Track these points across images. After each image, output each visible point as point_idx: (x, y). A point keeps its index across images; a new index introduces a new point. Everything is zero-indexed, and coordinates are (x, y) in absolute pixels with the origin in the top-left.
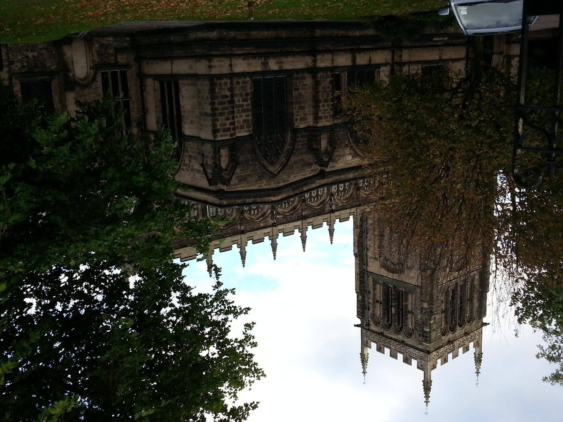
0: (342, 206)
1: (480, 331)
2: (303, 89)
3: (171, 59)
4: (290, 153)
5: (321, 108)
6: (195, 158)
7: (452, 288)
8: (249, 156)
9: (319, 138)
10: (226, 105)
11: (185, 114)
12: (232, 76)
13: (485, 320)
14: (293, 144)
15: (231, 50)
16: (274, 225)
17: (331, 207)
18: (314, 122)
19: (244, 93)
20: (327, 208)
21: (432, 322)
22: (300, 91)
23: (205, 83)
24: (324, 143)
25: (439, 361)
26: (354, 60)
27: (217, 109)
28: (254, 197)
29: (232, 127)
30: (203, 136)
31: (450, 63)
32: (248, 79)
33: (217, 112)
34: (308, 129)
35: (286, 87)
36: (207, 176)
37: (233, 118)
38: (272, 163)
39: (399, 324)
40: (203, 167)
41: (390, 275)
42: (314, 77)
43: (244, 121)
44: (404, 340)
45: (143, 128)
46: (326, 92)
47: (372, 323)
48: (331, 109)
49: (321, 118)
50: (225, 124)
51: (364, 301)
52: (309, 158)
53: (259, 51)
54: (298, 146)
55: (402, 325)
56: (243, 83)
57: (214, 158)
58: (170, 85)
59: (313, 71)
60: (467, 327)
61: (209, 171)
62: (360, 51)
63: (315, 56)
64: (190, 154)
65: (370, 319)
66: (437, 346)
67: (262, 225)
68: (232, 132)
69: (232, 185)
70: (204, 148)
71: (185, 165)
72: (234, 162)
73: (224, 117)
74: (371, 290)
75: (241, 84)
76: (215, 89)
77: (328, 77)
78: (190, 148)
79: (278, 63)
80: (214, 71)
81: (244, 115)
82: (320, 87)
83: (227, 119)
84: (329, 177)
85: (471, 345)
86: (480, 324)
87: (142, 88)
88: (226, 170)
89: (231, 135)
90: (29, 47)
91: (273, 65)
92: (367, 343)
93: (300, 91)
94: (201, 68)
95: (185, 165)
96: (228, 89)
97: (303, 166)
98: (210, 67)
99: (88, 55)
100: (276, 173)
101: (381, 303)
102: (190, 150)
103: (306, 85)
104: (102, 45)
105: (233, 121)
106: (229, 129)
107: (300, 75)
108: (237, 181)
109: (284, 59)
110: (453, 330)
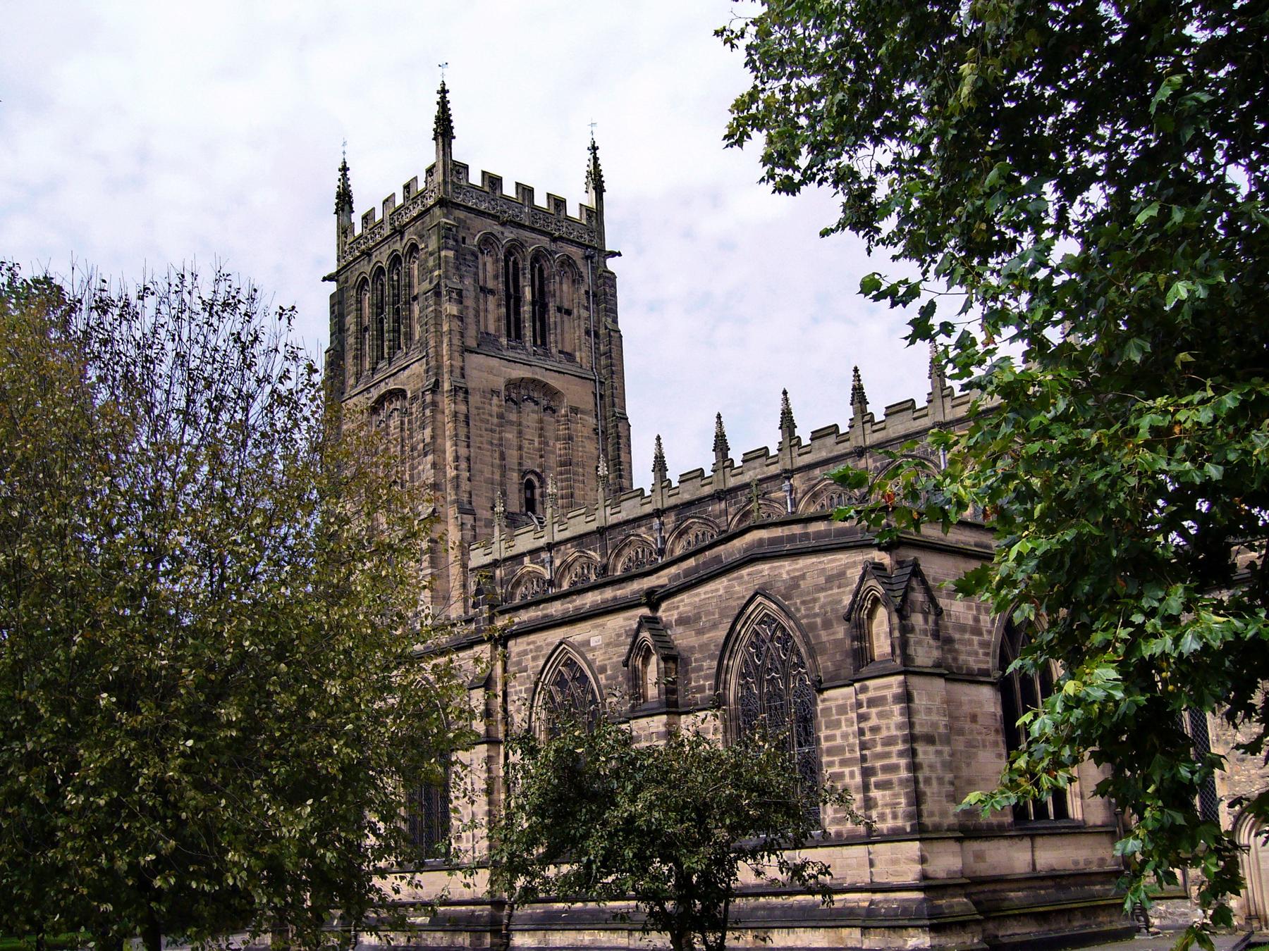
0: (639, 527)
1: (343, 263)
3: (1035, 879)
6: (962, 628)
7: (399, 354)
8: (824, 636)
10: (878, 764)
11: (992, 737)
12: (870, 837)
13: (332, 287)
14: (721, 671)
15: (872, 902)
16: (788, 474)
17: (662, 524)
20: (670, 520)
21: (436, 273)
23: (936, 819)
27: (901, 754)
29: (864, 710)
32: (832, 830)
33: (900, 747)
36: (924, 582)
37: (861, 732)
38: (767, 620)
40: (936, 606)
41: (540, 375)
43: (837, 724)
44: (500, 228)
50: (880, 715)
52: (682, 638)
54: (710, 665)
55: (506, 261)
60: (366, 268)
61: (919, 596)
64: (976, 638)
66: (427, 218)
67: (817, 472)
68: (862, 697)
70: (936, 654)
73: (884, 733)
78: (977, 654)
80: (914, 848)
81: (839, 741)
83: (875, 730)
84: (638, 592)
85: (358, 230)
88: (876, 601)
92: (589, 217)
96: (876, 805)
97: (697, 618)
100: (759, 599)
102: (976, 647)
105: (862, 725)
106: (872, 702)
110: (396, 260)
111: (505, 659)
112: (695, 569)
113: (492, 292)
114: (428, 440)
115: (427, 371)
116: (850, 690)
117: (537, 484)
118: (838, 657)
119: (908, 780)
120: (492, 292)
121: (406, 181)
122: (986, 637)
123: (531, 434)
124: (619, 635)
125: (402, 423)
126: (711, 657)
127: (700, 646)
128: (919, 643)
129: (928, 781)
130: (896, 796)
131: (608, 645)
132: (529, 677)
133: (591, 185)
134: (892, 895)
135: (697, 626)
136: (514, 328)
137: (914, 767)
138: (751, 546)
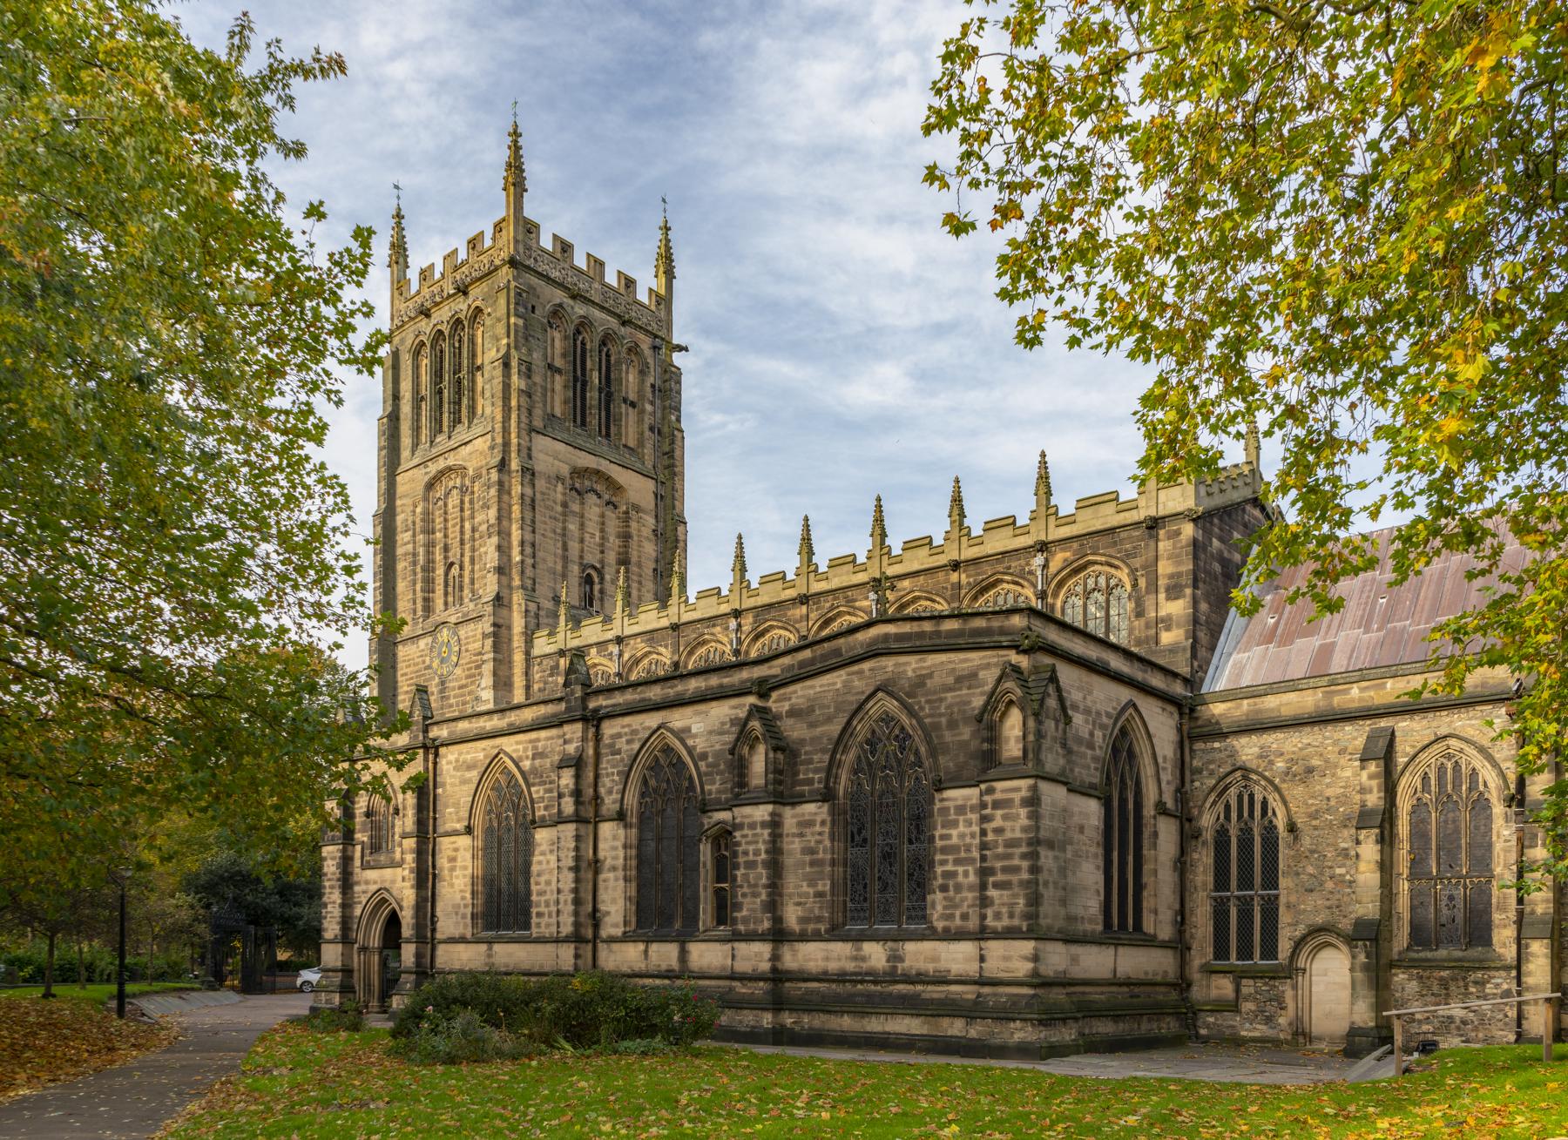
2: (807, 895)
4: (841, 742)
5: (762, 847)
6: (1079, 740)
7: (459, 428)
8: (948, 736)
9: (771, 776)
10: (998, 865)
11: (1093, 849)
12: (982, 934)
14: (833, 765)
15: (979, 995)
17: (739, 625)
18: (780, 815)
19: (951, 893)
20: (748, 622)
22: (811, 891)
23: (1049, 921)
24: (758, 764)
25: (488, 243)
26: (683, 955)
27: (1024, 856)
28: (938, 633)
29: (988, 811)
30: (1061, 791)
31: (469, 935)
33: (1024, 849)
34: (796, 801)
35: (845, 902)
36: (1059, 690)
37: (983, 833)
38: (887, 719)
39: (583, 343)
42: (778, 920)
43: (955, 824)
44: (571, 302)
45: (1187, 825)
46: (750, 886)
47: (647, 352)
48: (738, 844)
49: (764, 825)
50: (1005, 818)
51: (664, 408)
52: (794, 730)
53: (911, 987)
56: (951, 917)
57: (1040, 735)
58: (1121, 924)
59: (779, 936)
61: (1052, 703)
62: (668, 974)
63: (774, 970)
65: (650, 361)
68: (988, 798)
69: (996, 665)
71: (1103, 727)
72: (988, 723)
73: (1008, 835)
74: (647, 433)
75: (958, 913)
76: (1029, 904)
77: (745, 920)
78: (1089, 767)
79: (863, 959)
80: (1028, 947)
81: (955, 840)
82: (764, 897)
83: (999, 831)
86: (396, 340)
87: (1182, 917)
88: (1011, 702)
89: (991, 791)
90: (1458, 1028)
91: (876, 954)
92: (658, 304)
93: (811, 891)
94: (1057, 958)
95: (1103, 727)
96: (992, 904)
97: (811, 710)
98: (1036, 958)
99: (1306, 1001)
100: (880, 694)
101: (625, 400)
103: (799, 904)
104: (1269, 1020)
106: (997, 805)
107: (811, 927)
108: (982, 674)
109: (850, 966)
110: (457, 323)
111: (598, 738)
112: (812, 661)
113: (559, 371)
114: (492, 521)
115: (492, 448)
116: (975, 792)
117: (596, 580)
118: (961, 759)
119: (1029, 882)
120: (559, 371)
121: (471, 235)
122: (1098, 752)
123: (592, 527)
124: (723, 724)
125: (462, 502)
126: (823, 751)
127: (812, 739)
128: (1050, 749)
129: (1046, 884)
130: (1015, 896)
131: (710, 732)
132: (622, 760)
133: (662, 269)
134: (1001, 990)
135: (812, 718)
136: (579, 414)
137: (1035, 870)
138: (875, 640)
